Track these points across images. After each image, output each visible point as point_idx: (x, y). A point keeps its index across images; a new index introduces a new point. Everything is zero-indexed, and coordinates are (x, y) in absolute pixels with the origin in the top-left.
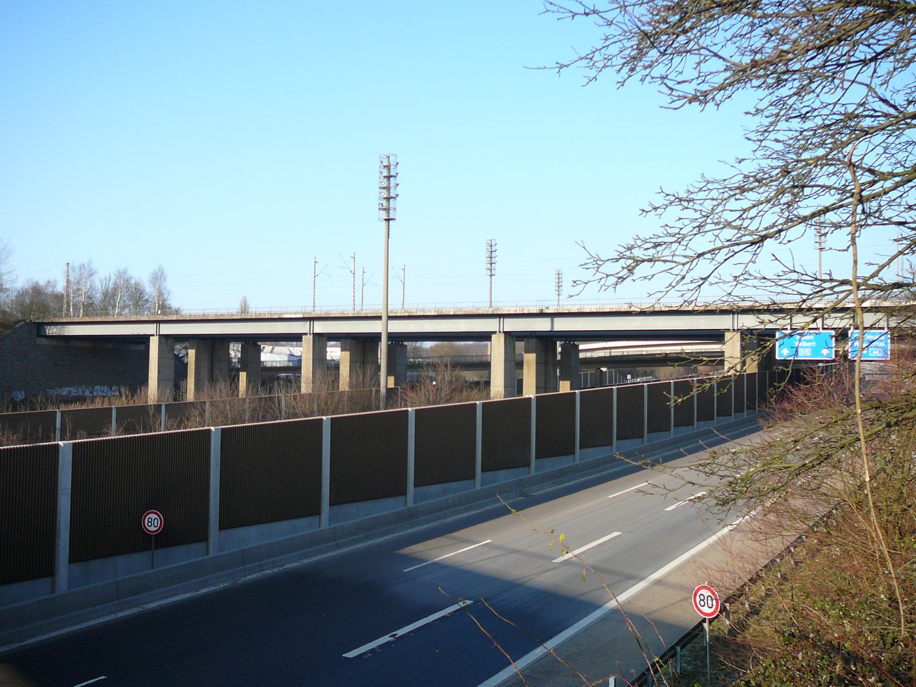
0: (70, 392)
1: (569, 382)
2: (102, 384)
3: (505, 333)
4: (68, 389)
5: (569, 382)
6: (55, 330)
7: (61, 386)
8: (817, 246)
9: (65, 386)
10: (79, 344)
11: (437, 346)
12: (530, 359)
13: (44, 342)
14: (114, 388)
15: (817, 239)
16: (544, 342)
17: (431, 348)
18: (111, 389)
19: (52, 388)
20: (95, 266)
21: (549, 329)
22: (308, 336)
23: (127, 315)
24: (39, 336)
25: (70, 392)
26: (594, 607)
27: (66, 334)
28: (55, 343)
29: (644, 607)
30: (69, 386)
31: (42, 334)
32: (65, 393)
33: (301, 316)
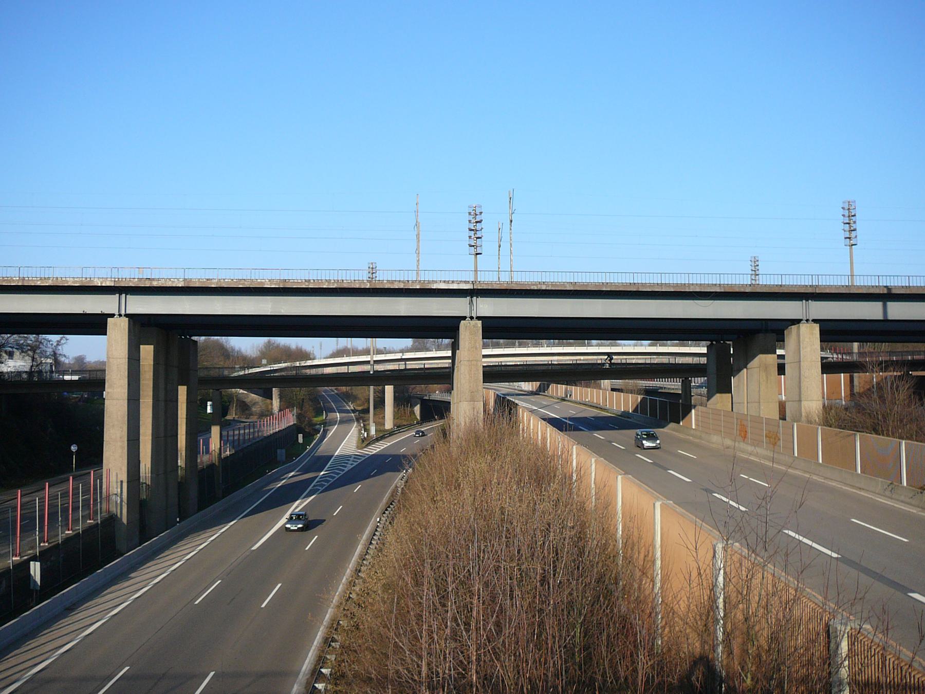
3: (126, 315)
15: (479, 226)
21: (880, 317)
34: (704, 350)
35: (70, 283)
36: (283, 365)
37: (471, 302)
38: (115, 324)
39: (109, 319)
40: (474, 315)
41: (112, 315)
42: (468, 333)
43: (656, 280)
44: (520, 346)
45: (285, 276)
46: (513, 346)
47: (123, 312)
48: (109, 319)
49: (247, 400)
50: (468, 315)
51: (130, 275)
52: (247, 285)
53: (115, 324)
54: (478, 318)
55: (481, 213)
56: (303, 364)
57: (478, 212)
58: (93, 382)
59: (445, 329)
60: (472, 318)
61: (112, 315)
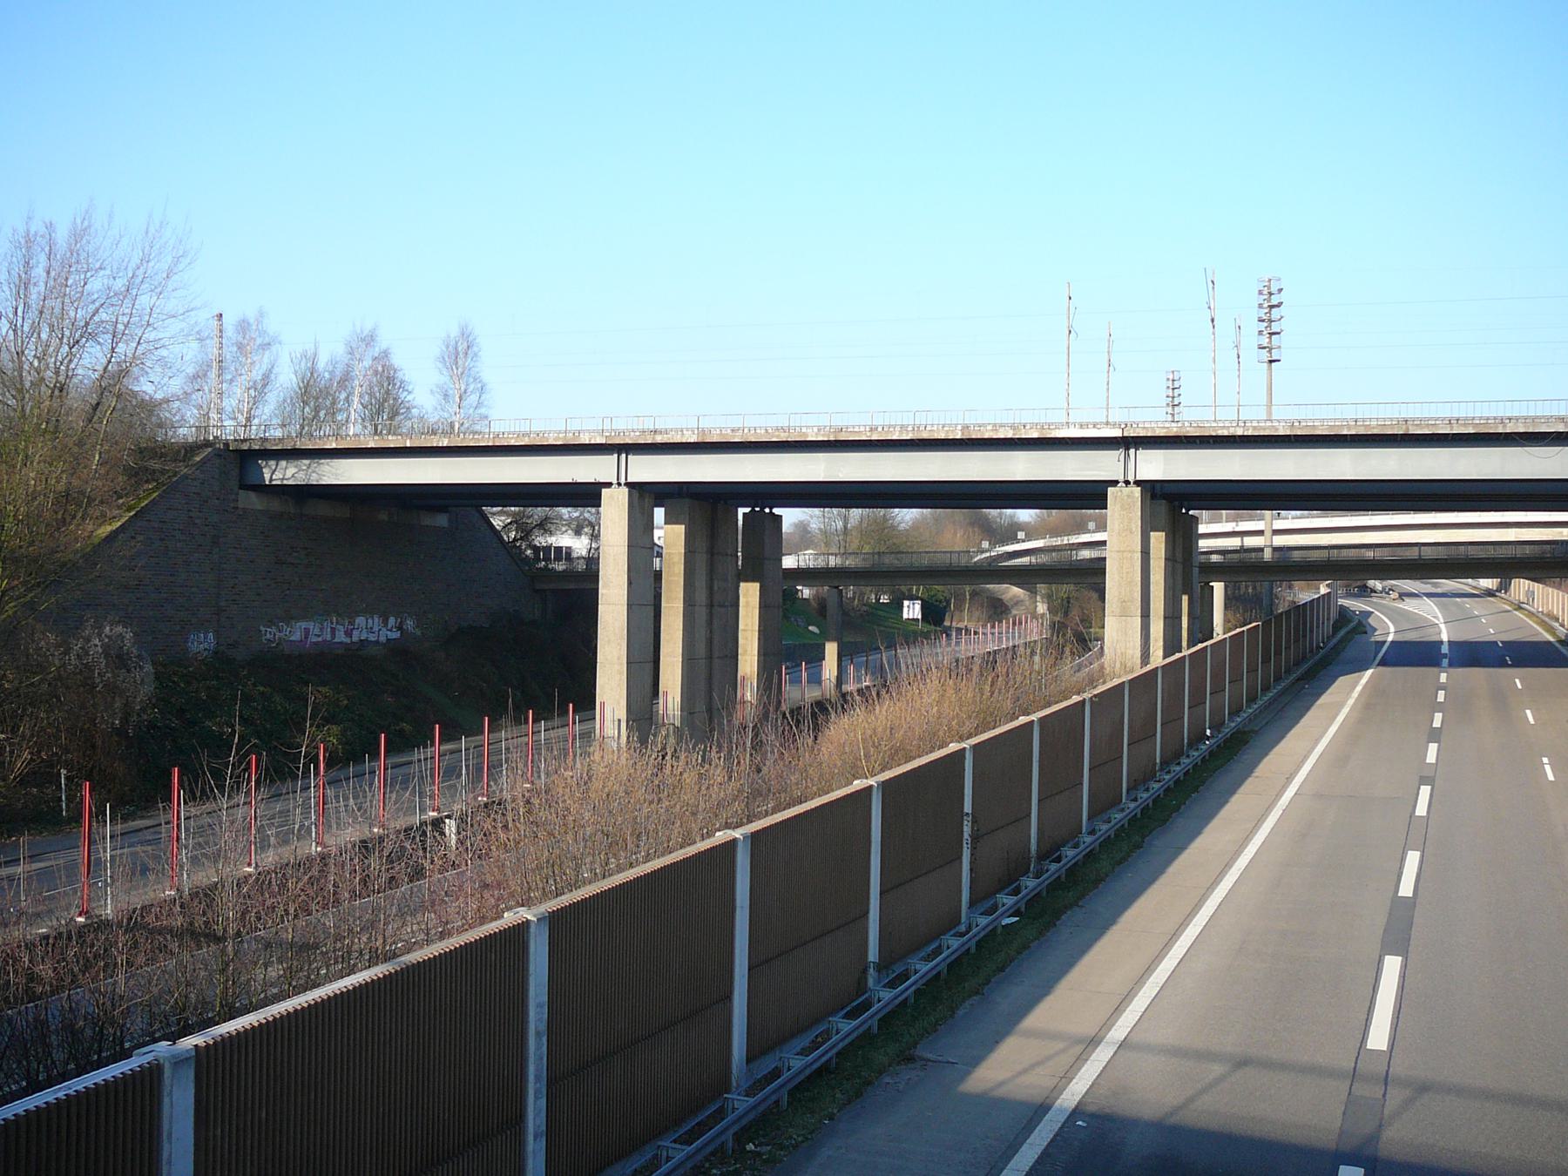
0: (307, 631)
1: (757, 585)
2: (369, 611)
3: (627, 484)
4: (304, 625)
5: (757, 585)
6: (291, 471)
7: (289, 618)
8: (1265, 354)
9: (298, 619)
10: (324, 509)
11: (924, 517)
12: (669, 535)
13: (252, 501)
14: (392, 621)
15: (1275, 313)
16: (703, 505)
17: (916, 526)
18: (386, 622)
19: (271, 623)
20: (272, 326)
22: (614, 490)
23: (356, 432)
24: (245, 487)
25: (307, 631)
26: (1042, 1109)
27: (326, 481)
28: (276, 505)
29: (1156, 1093)
30: (304, 618)
31: (252, 480)
32: (296, 637)
33: (1117, 433)
34: (1203, 544)
35: (585, 439)
36: (1039, 544)
37: (1127, 457)
38: (611, 497)
39: (604, 491)
40: (1131, 479)
41: (609, 485)
42: (1118, 507)
43: (1349, 413)
44: (1236, 520)
45: (839, 421)
46: (1218, 520)
47: (623, 481)
48: (604, 491)
49: (1006, 597)
50: (1121, 478)
51: (628, 428)
52: (783, 437)
53: (611, 497)
54: (1138, 483)
55: (1280, 290)
56: (1075, 539)
57: (1274, 289)
58: (589, 573)
59: (1091, 495)
60: (1127, 483)
61: (609, 485)
